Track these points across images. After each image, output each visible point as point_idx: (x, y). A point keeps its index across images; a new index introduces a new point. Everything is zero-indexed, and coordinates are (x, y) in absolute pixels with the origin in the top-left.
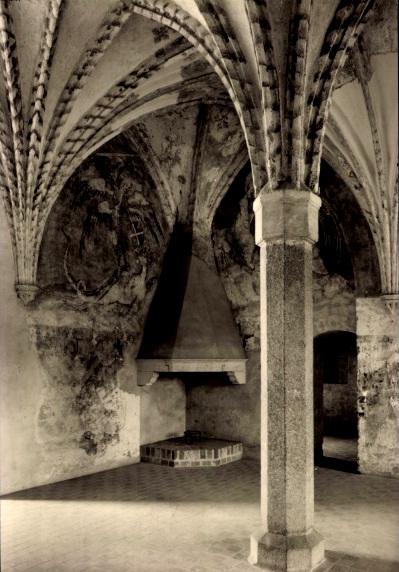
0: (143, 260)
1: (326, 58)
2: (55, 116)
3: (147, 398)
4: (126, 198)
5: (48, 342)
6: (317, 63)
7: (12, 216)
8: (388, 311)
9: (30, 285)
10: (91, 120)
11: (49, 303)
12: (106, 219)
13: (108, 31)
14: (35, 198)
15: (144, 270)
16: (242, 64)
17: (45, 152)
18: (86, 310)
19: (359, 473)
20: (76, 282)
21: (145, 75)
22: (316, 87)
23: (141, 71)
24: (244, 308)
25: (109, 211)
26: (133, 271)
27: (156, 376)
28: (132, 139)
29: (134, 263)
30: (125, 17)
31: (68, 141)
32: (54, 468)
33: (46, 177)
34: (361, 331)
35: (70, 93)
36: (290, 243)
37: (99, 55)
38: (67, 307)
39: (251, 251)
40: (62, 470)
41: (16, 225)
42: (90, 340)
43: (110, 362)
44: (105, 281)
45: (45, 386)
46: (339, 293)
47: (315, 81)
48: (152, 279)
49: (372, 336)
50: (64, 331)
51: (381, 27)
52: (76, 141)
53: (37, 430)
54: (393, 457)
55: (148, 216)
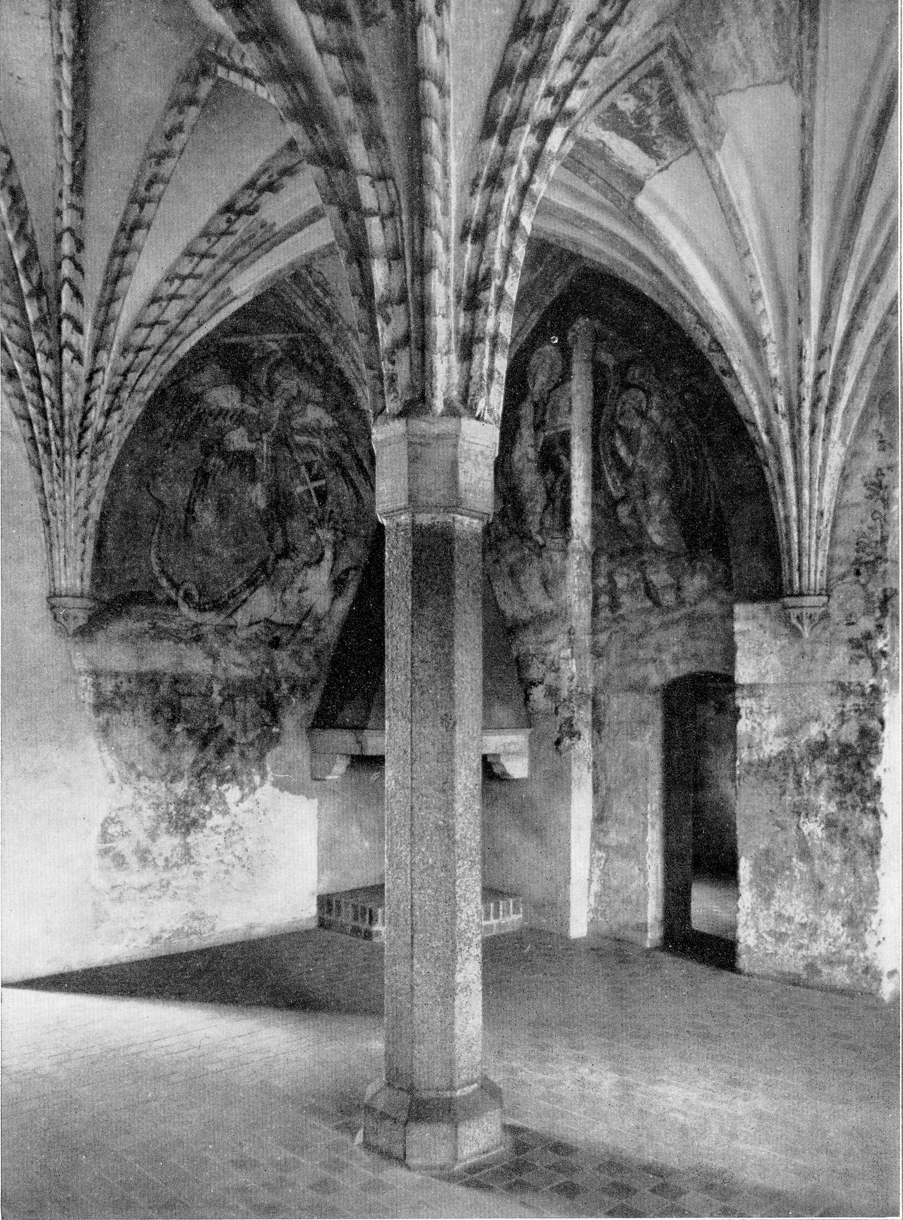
0: (326, 535)
1: (493, 144)
2: (105, 283)
3: (333, 806)
4: (286, 418)
5: (118, 702)
6: (475, 157)
7: (40, 472)
8: (796, 633)
9: (74, 596)
10: (177, 283)
11: (118, 627)
12: (245, 460)
13: (180, 118)
14: (81, 437)
15: (328, 554)
16: (341, 173)
17: (96, 350)
18: (198, 639)
19: (739, 972)
20: (176, 586)
21: (271, 187)
22: (477, 205)
23: (264, 180)
24: (525, 625)
25: (249, 446)
26: (304, 557)
27: (347, 762)
28: (299, 303)
29: (305, 545)
30: (205, 87)
31: (139, 325)
32: (130, 934)
33: (100, 398)
34: (744, 673)
35: (129, 238)
36: (424, 519)
37: (170, 163)
38: (159, 634)
39: (539, 509)
40: (147, 937)
41: (48, 487)
42: (207, 696)
43: (251, 736)
44: (239, 581)
45: (112, 781)
46: (707, 593)
47: (472, 194)
48: (346, 572)
49: (766, 686)
50: (152, 680)
51: (725, 37)
52: (152, 326)
53: (96, 861)
54: (806, 941)
55: (337, 448)
